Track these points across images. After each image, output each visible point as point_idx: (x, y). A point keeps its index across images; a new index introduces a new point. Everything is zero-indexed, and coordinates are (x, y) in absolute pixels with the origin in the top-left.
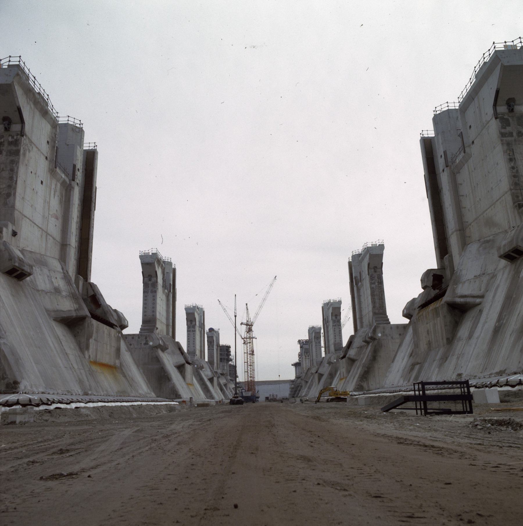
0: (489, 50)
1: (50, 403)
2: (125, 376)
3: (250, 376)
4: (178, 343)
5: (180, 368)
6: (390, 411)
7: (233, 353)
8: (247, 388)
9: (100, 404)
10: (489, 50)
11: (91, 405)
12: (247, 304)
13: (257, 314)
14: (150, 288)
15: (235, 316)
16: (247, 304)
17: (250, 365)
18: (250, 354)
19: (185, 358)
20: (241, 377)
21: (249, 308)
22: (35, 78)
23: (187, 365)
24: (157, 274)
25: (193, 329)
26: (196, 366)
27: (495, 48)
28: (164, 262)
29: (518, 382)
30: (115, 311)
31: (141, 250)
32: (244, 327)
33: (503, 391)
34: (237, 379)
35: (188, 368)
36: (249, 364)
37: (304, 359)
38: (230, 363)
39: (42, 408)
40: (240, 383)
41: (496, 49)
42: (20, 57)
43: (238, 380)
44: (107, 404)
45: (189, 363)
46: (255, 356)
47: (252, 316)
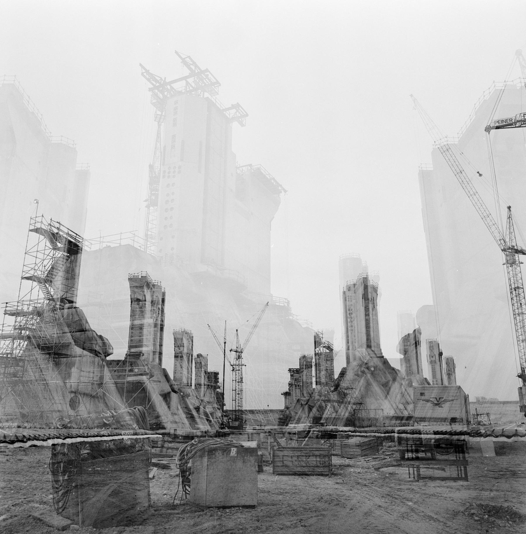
0: (489, 88)
1: (25, 440)
3: (237, 405)
4: (164, 370)
5: (166, 397)
6: (381, 470)
7: (221, 380)
8: (234, 417)
9: (79, 440)
10: (489, 88)
11: (69, 441)
13: (247, 341)
15: (225, 343)
16: (237, 330)
17: (238, 394)
18: (238, 382)
19: (171, 386)
20: (229, 405)
21: (239, 335)
22: (29, 97)
23: (173, 394)
24: (144, 295)
26: (182, 394)
27: (495, 86)
28: (154, 286)
29: (514, 433)
30: (101, 337)
31: (131, 273)
32: (234, 353)
33: (498, 442)
34: (224, 407)
35: (174, 396)
36: (237, 393)
37: (294, 388)
38: (218, 390)
39: (17, 445)
40: (227, 411)
41: (496, 88)
42: (15, 76)
43: (225, 408)
44: (86, 440)
45: (175, 392)
46: (243, 384)
47: (242, 341)
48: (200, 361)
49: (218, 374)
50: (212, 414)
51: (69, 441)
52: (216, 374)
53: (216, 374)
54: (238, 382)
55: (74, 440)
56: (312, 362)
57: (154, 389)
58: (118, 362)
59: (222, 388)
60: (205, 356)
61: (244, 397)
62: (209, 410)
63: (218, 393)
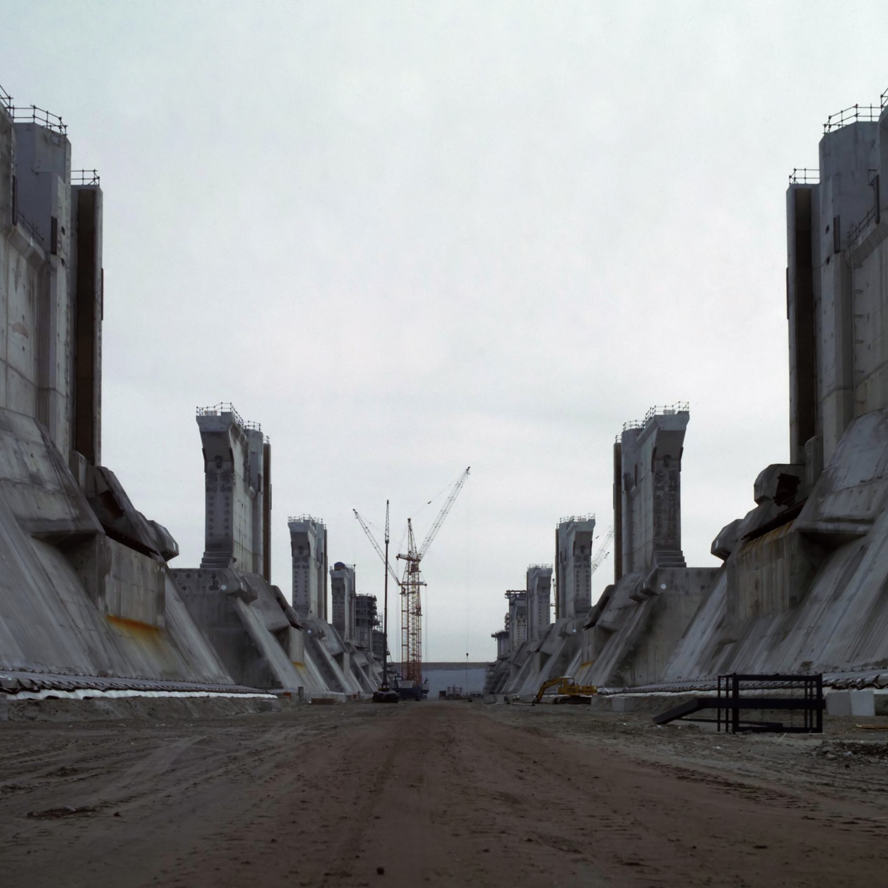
1: (36, 688)
2: (175, 645)
3: (411, 652)
4: (275, 589)
5: (281, 635)
7: (380, 610)
11: (113, 694)
12: (409, 520)
13: (429, 540)
14: (220, 482)
15: (387, 542)
16: (409, 520)
17: (413, 634)
19: (289, 616)
20: (396, 655)
21: (413, 527)
24: (232, 454)
25: (305, 564)
26: (310, 632)
30: (152, 523)
34: (388, 657)
36: (411, 632)
38: (376, 628)
43: (389, 660)
46: (423, 618)
48: (343, 575)
49: (374, 599)
50: (365, 668)
51: (113, 694)
52: (371, 600)
53: (371, 600)
54: (413, 613)
55: (122, 694)
56: (550, 578)
57: (259, 621)
58: (188, 572)
59: (382, 624)
60: (350, 567)
61: (423, 628)
62: (360, 660)
63: (376, 633)
